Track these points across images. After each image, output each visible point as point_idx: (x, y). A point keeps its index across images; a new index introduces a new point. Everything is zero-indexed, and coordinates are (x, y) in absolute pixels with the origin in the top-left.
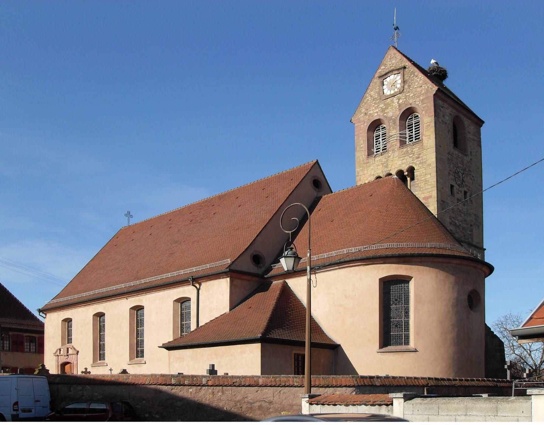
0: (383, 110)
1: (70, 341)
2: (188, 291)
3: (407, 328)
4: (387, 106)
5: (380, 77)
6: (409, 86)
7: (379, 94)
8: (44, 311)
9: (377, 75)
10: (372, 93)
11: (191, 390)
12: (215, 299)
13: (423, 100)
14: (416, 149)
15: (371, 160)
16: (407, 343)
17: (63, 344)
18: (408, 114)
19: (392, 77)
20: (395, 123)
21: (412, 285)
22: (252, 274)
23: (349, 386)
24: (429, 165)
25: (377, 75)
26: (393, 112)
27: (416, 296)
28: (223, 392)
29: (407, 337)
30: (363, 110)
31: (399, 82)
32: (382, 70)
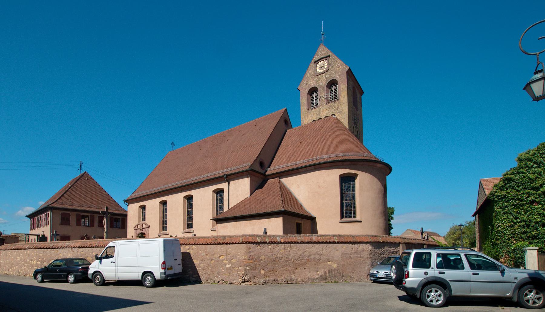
0: (317, 82)
1: (144, 219)
2: (224, 186)
3: (354, 207)
4: (319, 79)
5: (315, 62)
6: (332, 67)
7: (314, 71)
8: (129, 201)
9: (313, 61)
10: (310, 71)
11: (270, 247)
12: (239, 191)
13: (340, 75)
14: (336, 104)
15: (310, 111)
16: (354, 216)
17: (139, 221)
18: (332, 84)
19: (322, 62)
20: (323, 89)
21: (357, 181)
22: (259, 175)
23: (366, 243)
24: (344, 113)
25: (313, 61)
26: (322, 83)
27: (361, 186)
28: (291, 248)
29: (354, 212)
30: (305, 82)
31: (326, 64)
32: (316, 58)
